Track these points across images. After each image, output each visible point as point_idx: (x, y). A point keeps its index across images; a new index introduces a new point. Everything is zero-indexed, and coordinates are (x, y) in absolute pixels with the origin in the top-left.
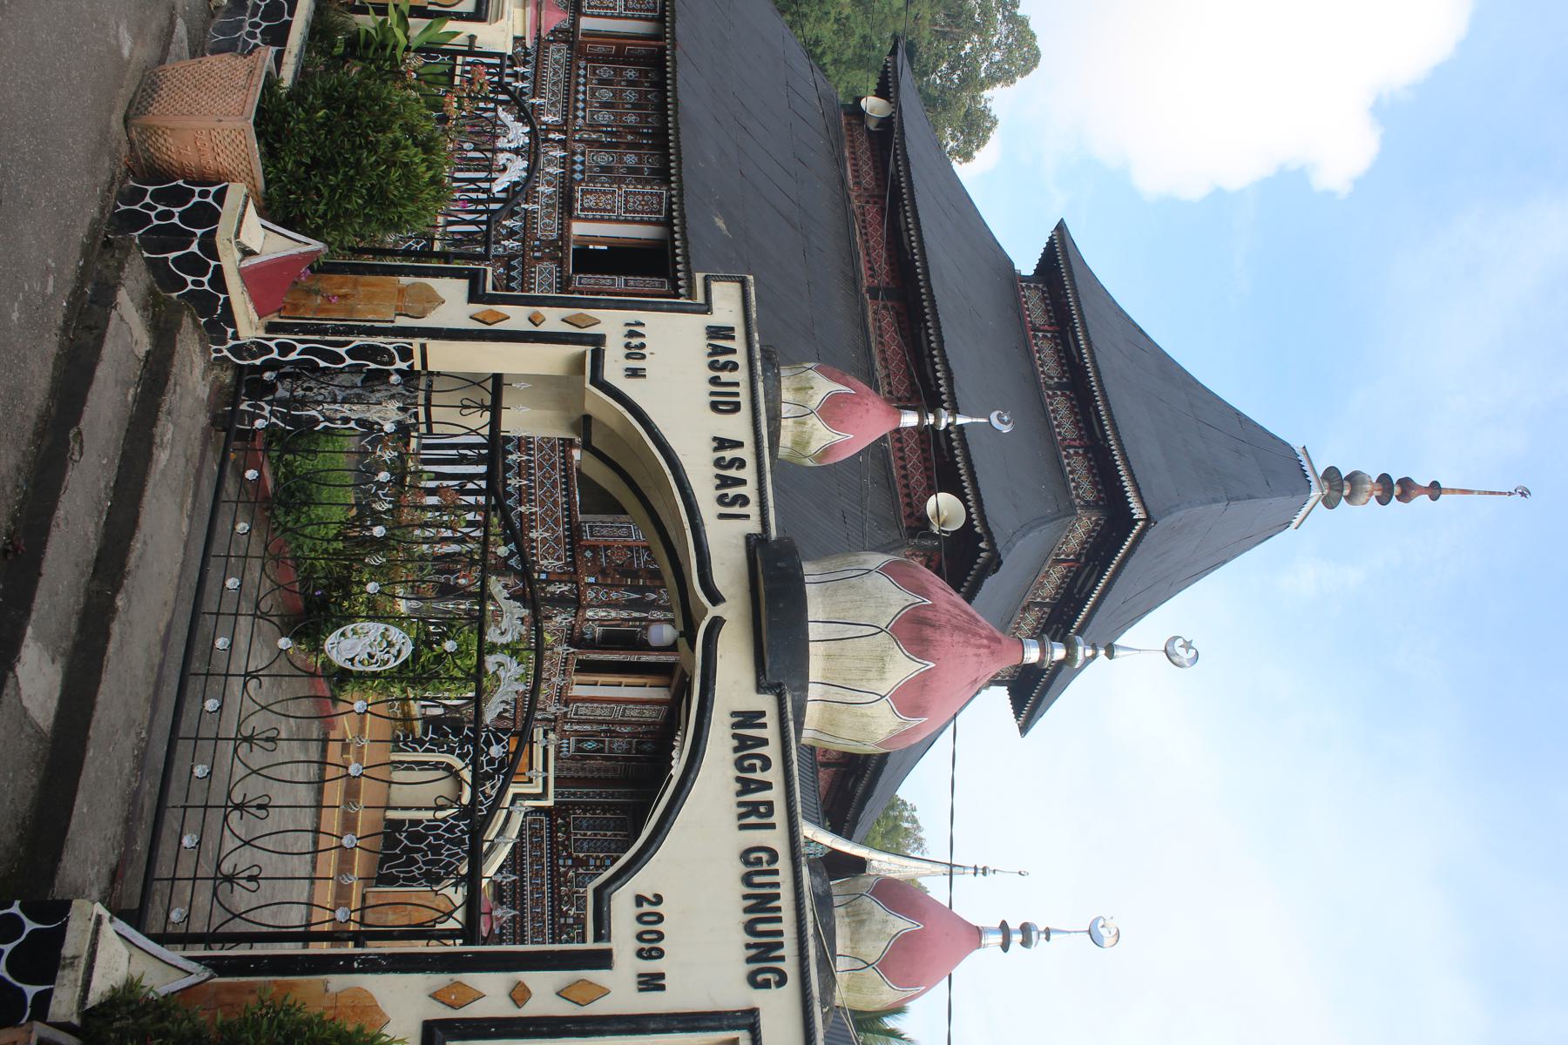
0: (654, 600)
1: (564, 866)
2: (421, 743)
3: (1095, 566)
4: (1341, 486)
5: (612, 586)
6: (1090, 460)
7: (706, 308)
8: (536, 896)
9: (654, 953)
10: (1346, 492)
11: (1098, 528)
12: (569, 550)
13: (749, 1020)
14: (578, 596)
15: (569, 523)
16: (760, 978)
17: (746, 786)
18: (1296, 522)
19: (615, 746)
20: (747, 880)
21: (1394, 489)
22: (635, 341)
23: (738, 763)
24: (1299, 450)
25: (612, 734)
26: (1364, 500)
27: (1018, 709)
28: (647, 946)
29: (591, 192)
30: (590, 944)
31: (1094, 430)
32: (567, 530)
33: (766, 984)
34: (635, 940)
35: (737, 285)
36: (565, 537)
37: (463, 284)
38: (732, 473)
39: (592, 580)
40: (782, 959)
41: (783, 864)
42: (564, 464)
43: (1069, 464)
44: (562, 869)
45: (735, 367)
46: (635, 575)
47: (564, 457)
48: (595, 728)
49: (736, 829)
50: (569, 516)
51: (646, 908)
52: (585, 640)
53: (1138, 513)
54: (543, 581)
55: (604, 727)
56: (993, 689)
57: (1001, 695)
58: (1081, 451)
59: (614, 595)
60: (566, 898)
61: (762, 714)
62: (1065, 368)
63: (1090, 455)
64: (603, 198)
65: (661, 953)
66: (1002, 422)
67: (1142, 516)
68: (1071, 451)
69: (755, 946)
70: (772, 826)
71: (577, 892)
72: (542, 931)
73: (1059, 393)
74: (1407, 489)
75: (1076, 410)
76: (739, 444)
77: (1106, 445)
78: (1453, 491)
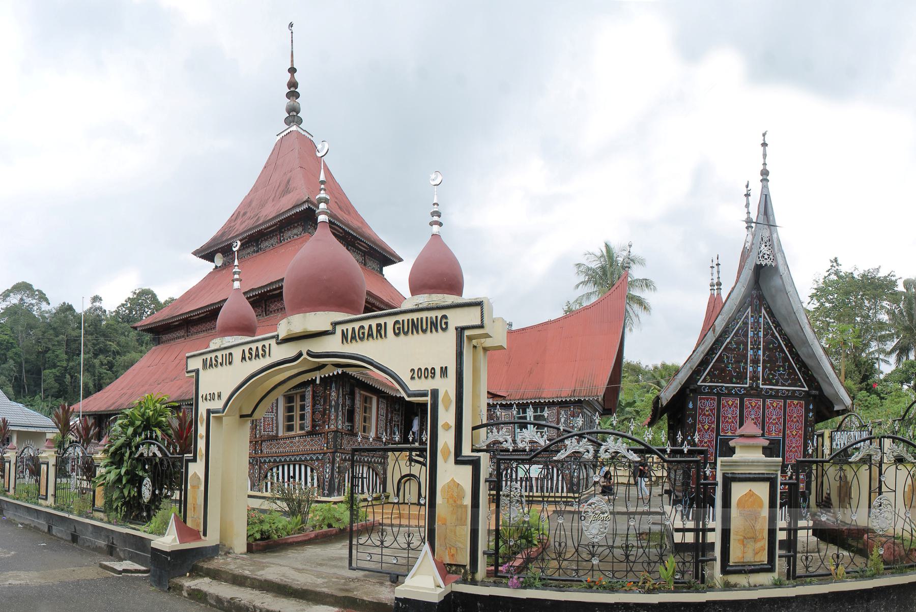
0: (335, 402)
4: (293, 115)
5: (329, 419)
6: (285, 230)
9: (433, 372)
10: (295, 114)
13: (461, 330)
15: (305, 436)
16: (444, 326)
17: (370, 335)
18: (310, 137)
19: (396, 420)
20: (406, 333)
21: (293, 94)
22: (208, 397)
23: (362, 339)
24: (279, 138)
27: (392, 262)
28: (430, 374)
30: (428, 399)
31: (273, 229)
33: (446, 323)
34: (429, 380)
37: (190, 464)
39: (327, 426)
40: (436, 317)
42: (284, 439)
43: (287, 239)
46: (325, 410)
47: (282, 439)
48: (389, 427)
50: (303, 436)
51: (416, 375)
53: (305, 206)
56: (384, 272)
58: (282, 234)
59: (333, 417)
61: (343, 331)
63: (283, 230)
68: (282, 239)
69: (431, 329)
70: (385, 323)
74: (293, 84)
75: (266, 238)
78: (292, 61)
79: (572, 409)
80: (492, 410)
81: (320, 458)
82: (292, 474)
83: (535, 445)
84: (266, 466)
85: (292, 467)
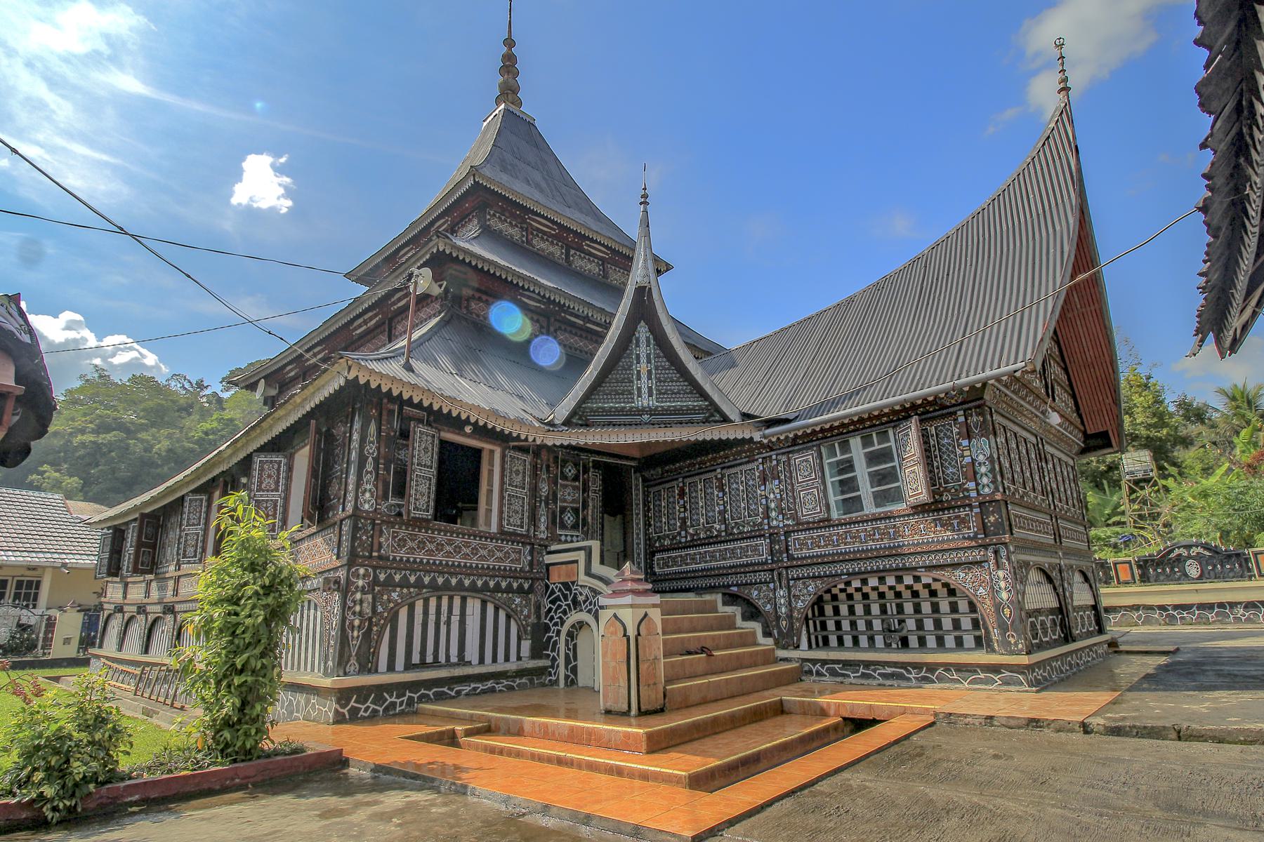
1: (686, 537)
2: (554, 659)
3: (529, 218)
4: (509, 92)
8: (708, 558)
29: (185, 551)
44: (689, 539)
60: (708, 533)
64: (189, 542)
71: (703, 524)
72: (732, 550)
79: (961, 419)
80: (774, 457)
81: (526, 586)
83: (882, 526)
85: (445, 601)
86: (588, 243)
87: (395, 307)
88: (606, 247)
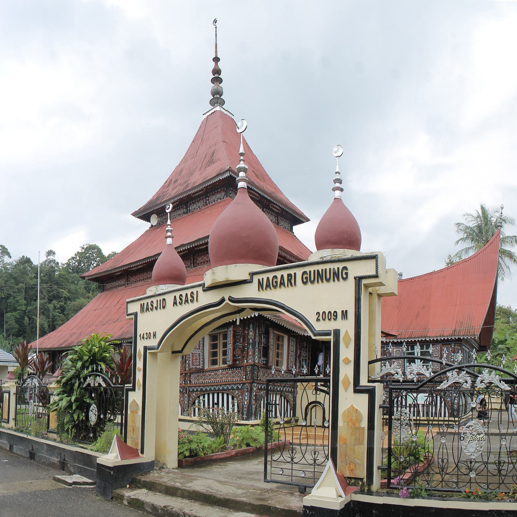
5: (248, 354)
6: (210, 195)
7: (136, 314)
9: (335, 314)
10: (218, 96)
11: (234, 190)
12: (236, 369)
13: (359, 280)
14: (251, 365)
15: (227, 369)
18: (231, 116)
19: (304, 355)
22: (145, 336)
23: (275, 287)
24: (205, 116)
25: (300, 355)
26: (221, 88)
28: (333, 317)
32: (229, 369)
33: (346, 274)
35: (129, 305)
36: (232, 370)
38: (184, 299)
39: (245, 361)
40: (338, 268)
41: (307, 269)
43: (212, 203)
45: (152, 302)
49: (296, 287)
51: (321, 318)
52: (266, 363)
53: (227, 174)
54: (246, 377)
55: (298, 359)
57: (297, 229)
58: (207, 198)
59: (250, 353)
61: (259, 280)
62: (181, 207)
63: (209, 195)
65: (335, 312)
66: (169, 208)
67: (229, 173)
68: (207, 202)
70: (295, 274)
73: (189, 208)
74: (217, 71)
76: (175, 297)
77: (205, 189)
78: (216, 52)
79: (453, 346)
80: (386, 347)
81: (240, 387)
82: (216, 401)
83: (422, 377)
84: (194, 394)
86: (272, 204)
87: (198, 248)
88: (280, 207)
